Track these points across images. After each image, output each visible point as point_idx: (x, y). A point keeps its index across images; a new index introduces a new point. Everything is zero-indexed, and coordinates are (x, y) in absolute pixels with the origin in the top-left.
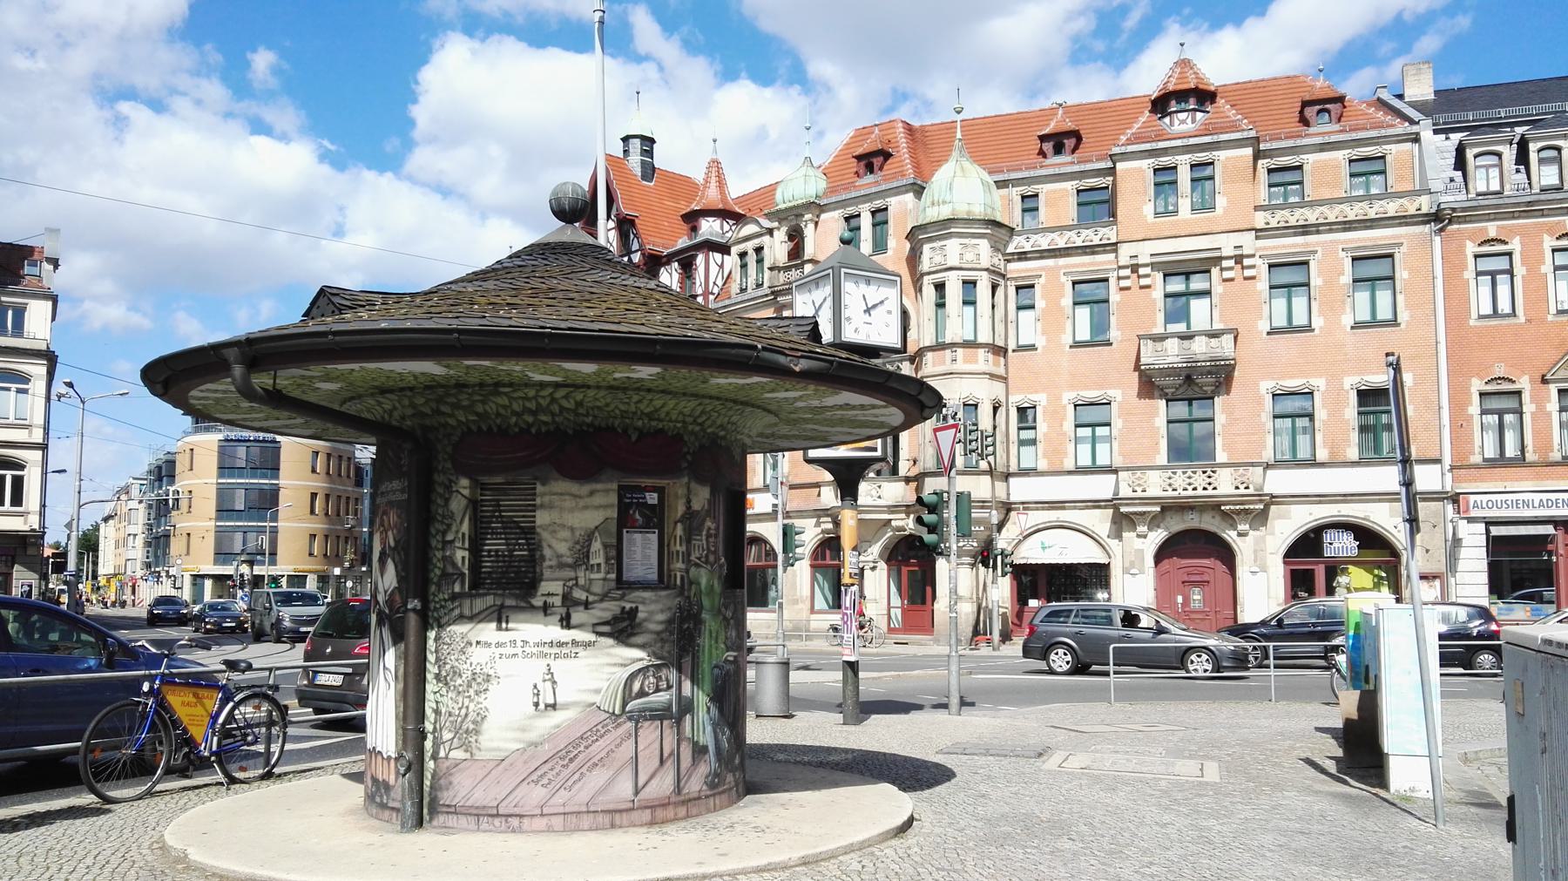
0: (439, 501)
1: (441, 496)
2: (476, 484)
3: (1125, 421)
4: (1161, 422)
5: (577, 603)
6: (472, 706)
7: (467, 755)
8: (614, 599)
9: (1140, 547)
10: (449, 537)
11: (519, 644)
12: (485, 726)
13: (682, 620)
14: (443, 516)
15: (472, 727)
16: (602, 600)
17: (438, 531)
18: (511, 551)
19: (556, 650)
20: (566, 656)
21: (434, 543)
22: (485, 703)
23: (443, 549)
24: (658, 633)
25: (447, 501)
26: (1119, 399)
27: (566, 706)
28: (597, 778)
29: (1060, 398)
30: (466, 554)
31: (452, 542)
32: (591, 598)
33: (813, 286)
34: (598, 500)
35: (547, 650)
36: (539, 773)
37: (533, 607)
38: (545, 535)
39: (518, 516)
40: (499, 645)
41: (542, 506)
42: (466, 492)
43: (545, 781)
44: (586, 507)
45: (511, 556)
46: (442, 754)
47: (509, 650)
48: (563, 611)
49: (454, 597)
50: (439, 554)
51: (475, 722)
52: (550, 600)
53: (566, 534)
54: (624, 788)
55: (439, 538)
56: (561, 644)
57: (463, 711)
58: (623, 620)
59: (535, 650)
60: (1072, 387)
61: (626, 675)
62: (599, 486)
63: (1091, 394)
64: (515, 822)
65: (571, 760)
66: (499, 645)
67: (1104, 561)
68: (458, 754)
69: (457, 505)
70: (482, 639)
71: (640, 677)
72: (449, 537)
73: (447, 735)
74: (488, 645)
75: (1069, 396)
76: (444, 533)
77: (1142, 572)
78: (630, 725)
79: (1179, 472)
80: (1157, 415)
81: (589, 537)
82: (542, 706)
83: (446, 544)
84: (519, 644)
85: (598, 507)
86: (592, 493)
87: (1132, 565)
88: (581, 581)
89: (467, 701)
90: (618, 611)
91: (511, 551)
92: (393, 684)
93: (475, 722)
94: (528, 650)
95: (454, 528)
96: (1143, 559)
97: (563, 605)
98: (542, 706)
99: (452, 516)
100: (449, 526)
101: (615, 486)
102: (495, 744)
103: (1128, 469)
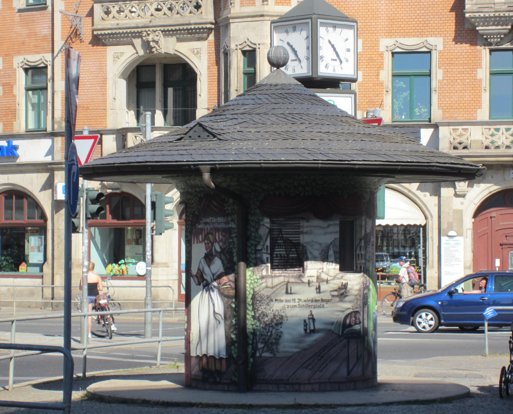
0: (252, 229)
1: (253, 227)
2: (272, 222)
3: (446, 72)
4: (483, 73)
5: (323, 281)
6: (274, 331)
7: (272, 355)
8: (339, 279)
9: (460, 207)
10: (259, 247)
11: (297, 300)
12: (281, 340)
13: (364, 289)
14: (255, 237)
15: (274, 341)
16: (333, 279)
17: (252, 245)
18: (288, 255)
19: (314, 304)
20: (319, 307)
21: (249, 250)
22: (281, 330)
23: (255, 253)
24: (356, 296)
25: (257, 230)
26: (440, 47)
27: (319, 331)
28: (333, 367)
29: (376, 44)
30: (269, 256)
31: (261, 250)
32: (329, 278)
33: (290, 29)
34: (331, 229)
35: (310, 304)
36: (308, 363)
37: (303, 282)
38: (309, 247)
39: (292, 238)
40: (287, 301)
41: (306, 233)
42: (268, 225)
43: (310, 367)
44: (326, 233)
45: (288, 257)
46: (258, 354)
47: (292, 304)
48: (317, 284)
49: (262, 278)
50: (253, 256)
51: (275, 339)
52: (311, 279)
53: (317, 246)
54: (343, 372)
55: (253, 248)
56: (316, 301)
57: (269, 334)
58: (343, 289)
59: (304, 304)
60: (389, 34)
61: (343, 316)
62: (331, 222)
63: (411, 42)
64: (297, 387)
65: (322, 357)
66: (287, 301)
67: (418, 220)
68: (266, 355)
69: (263, 231)
70: (278, 298)
71: (349, 317)
72: (259, 247)
73: (260, 346)
74: (281, 301)
75: (386, 44)
76: (256, 246)
77: (460, 234)
78: (345, 341)
79: (503, 128)
80: (479, 65)
81: (328, 247)
82: (308, 331)
83: (256, 251)
84: (297, 300)
85: (331, 233)
86: (329, 226)
87: (450, 227)
88: (325, 270)
89: (271, 329)
90: (340, 285)
91: (288, 255)
92: (222, 322)
93: (275, 339)
94: (301, 303)
95: (262, 243)
96: (461, 221)
97: (317, 281)
98: (308, 331)
99: (260, 237)
100: (259, 242)
101: (338, 222)
102: (286, 349)
103: (449, 124)
